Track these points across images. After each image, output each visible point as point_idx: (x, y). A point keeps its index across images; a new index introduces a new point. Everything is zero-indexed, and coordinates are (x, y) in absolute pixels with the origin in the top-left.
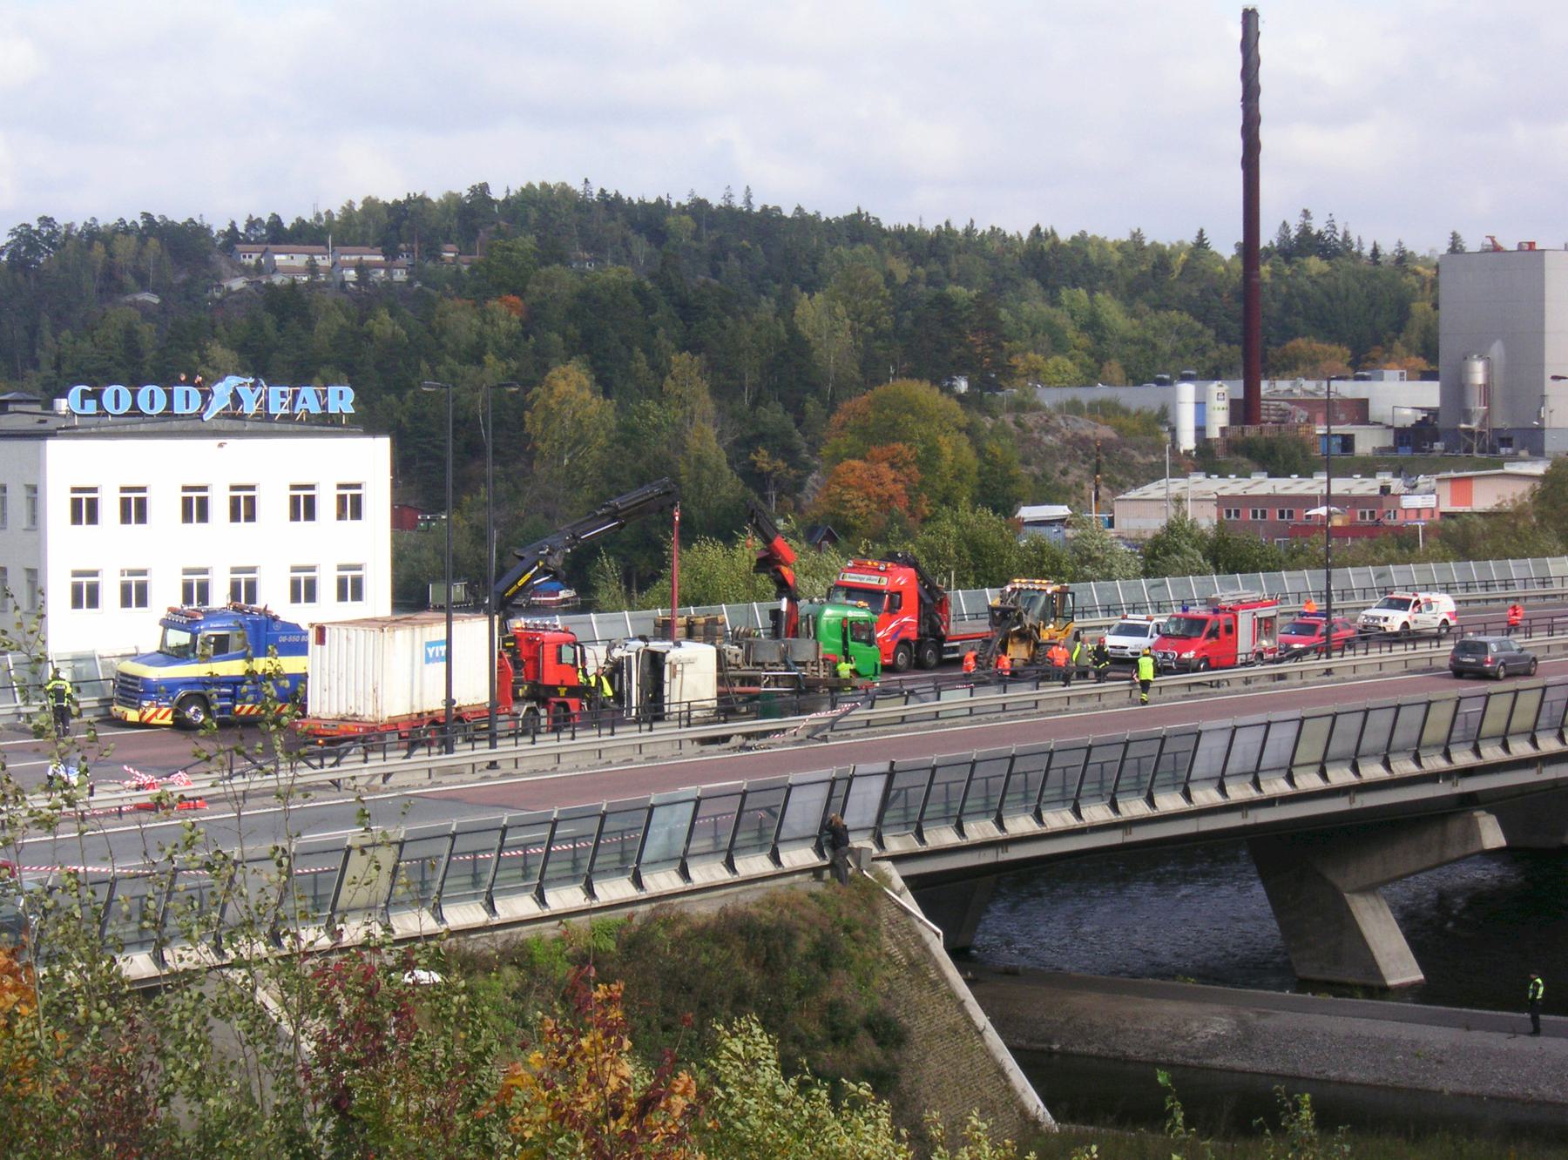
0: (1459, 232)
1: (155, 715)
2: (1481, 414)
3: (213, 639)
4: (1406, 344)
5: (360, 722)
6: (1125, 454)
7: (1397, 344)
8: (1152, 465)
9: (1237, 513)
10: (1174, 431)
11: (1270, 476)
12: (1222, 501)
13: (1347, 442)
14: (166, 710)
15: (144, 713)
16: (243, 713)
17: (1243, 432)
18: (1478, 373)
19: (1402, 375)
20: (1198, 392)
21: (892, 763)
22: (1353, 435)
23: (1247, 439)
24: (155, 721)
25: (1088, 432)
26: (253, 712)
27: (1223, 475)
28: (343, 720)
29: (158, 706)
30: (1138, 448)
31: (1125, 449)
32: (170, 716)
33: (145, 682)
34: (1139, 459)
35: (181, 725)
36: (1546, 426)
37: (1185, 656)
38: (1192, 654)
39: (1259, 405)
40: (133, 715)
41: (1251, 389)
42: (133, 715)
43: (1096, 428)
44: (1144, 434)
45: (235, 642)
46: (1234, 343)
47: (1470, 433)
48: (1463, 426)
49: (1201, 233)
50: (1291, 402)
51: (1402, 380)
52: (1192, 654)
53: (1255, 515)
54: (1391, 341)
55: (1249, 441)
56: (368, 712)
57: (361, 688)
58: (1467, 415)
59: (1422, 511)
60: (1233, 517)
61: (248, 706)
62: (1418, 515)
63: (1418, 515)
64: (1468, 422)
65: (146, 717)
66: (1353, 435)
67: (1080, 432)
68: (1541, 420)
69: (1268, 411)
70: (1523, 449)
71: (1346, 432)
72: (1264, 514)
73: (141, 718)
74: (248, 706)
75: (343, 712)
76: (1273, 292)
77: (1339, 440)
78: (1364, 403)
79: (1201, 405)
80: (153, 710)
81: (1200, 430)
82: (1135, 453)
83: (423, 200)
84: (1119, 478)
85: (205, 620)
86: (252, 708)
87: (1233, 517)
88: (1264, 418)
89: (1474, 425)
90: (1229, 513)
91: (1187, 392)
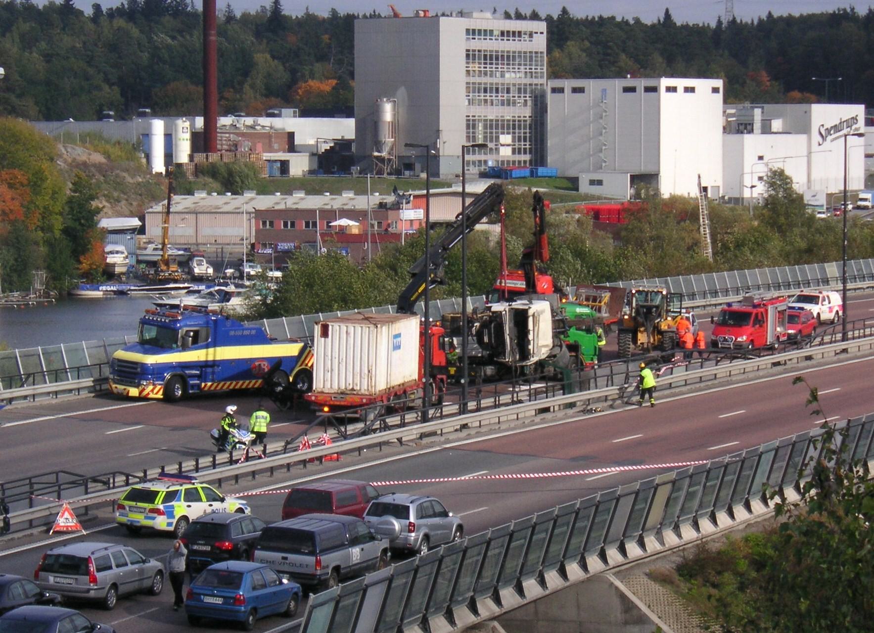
0: (566, 6)
1: (152, 391)
2: (390, 145)
3: (192, 334)
4: (252, 87)
5: (358, 394)
6: (117, 176)
7: (246, 87)
8: (139, 184)
9: (271, 224)
10: (148, 157)
11: (258, 194)
12: (259, 214)
13: (284, 166)
14: (160, 387)
15: (144, 390)
16: (206, 389)
17: (207, 158)
18: (388, 112)
19: (295, 112)
20: (166, 127)
21: (849, 421)
22: (288, 161)
23: (211, 163)
24: (151, 396)
25: (84, 158)
26: (212, 388)
27: (190, 193)
28: (342, 393)
29: (154, 384)
30: (127, 170)
31: (118, 171)
32: (161, 392)
33: (143, 365)
34: (129, 179)
35: (168, 398)
36: (441, 154)
37: (739, 339)
38: (745, 338)
39: (217, 136)
40: (134, 392)
41: (210, 124)
42: (134, 392)
43: (90, 154)
44: (128, 159)
45: (203, 334)
46: (113, 84)
47: (381, 160)
48: (376, 154)
49: (517, 9)
50: (237, 134)
51: (295, 116)
52: (745, 338)
53: (286, 225)
54: (241, 84)
55: (213, 166)
56: (363, 387)
57: (358, 369)
58: (378, 145)
59: (414, 222)
60: (268, 227)
61: (209, 384)
62: (411, 225)
63: (411, 225)
64: (379, 152)
65: (145, 393)
66: (288, 161)
67: (78, 158)
68: (438, 150)
69: (223, 141)
70: (422, 172)
71: (283, 159)
72: (293, 225)
73: (140, 393)
74: (209, 384)
75: (343, 387)
76: (139, 44)
77: (279, 165)
78: (291, 135)
79: (169, 138)
80: (151, 387)
81: (169, 156)
82: (125, 174)
83: (823, 13)
84: (116, 194)
85: (183, 319)
86: (211, 386)
87: (268, 227)
88: (219, 147)
89: (384, 154)
90: (264, 223)
91: (158, 126)
